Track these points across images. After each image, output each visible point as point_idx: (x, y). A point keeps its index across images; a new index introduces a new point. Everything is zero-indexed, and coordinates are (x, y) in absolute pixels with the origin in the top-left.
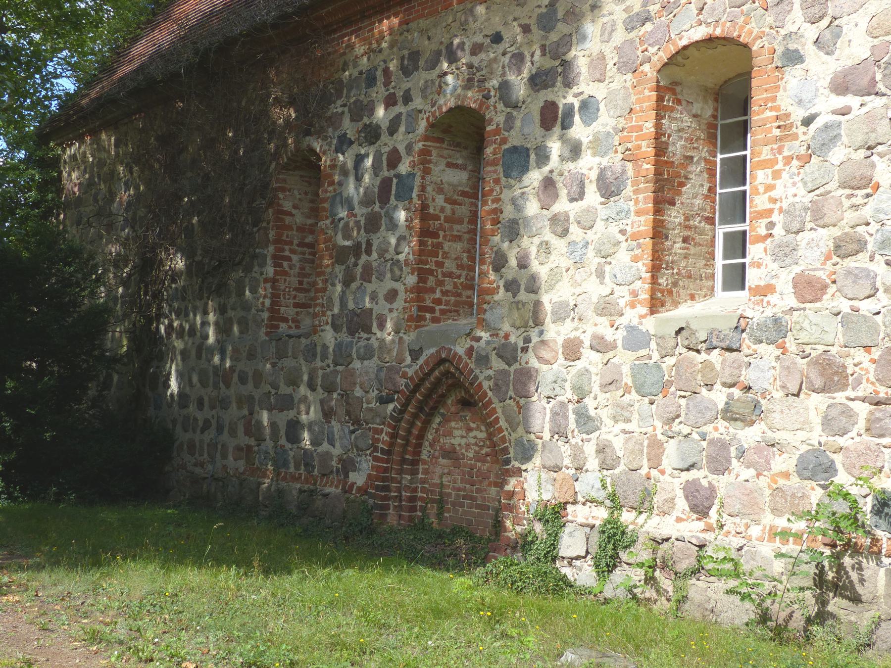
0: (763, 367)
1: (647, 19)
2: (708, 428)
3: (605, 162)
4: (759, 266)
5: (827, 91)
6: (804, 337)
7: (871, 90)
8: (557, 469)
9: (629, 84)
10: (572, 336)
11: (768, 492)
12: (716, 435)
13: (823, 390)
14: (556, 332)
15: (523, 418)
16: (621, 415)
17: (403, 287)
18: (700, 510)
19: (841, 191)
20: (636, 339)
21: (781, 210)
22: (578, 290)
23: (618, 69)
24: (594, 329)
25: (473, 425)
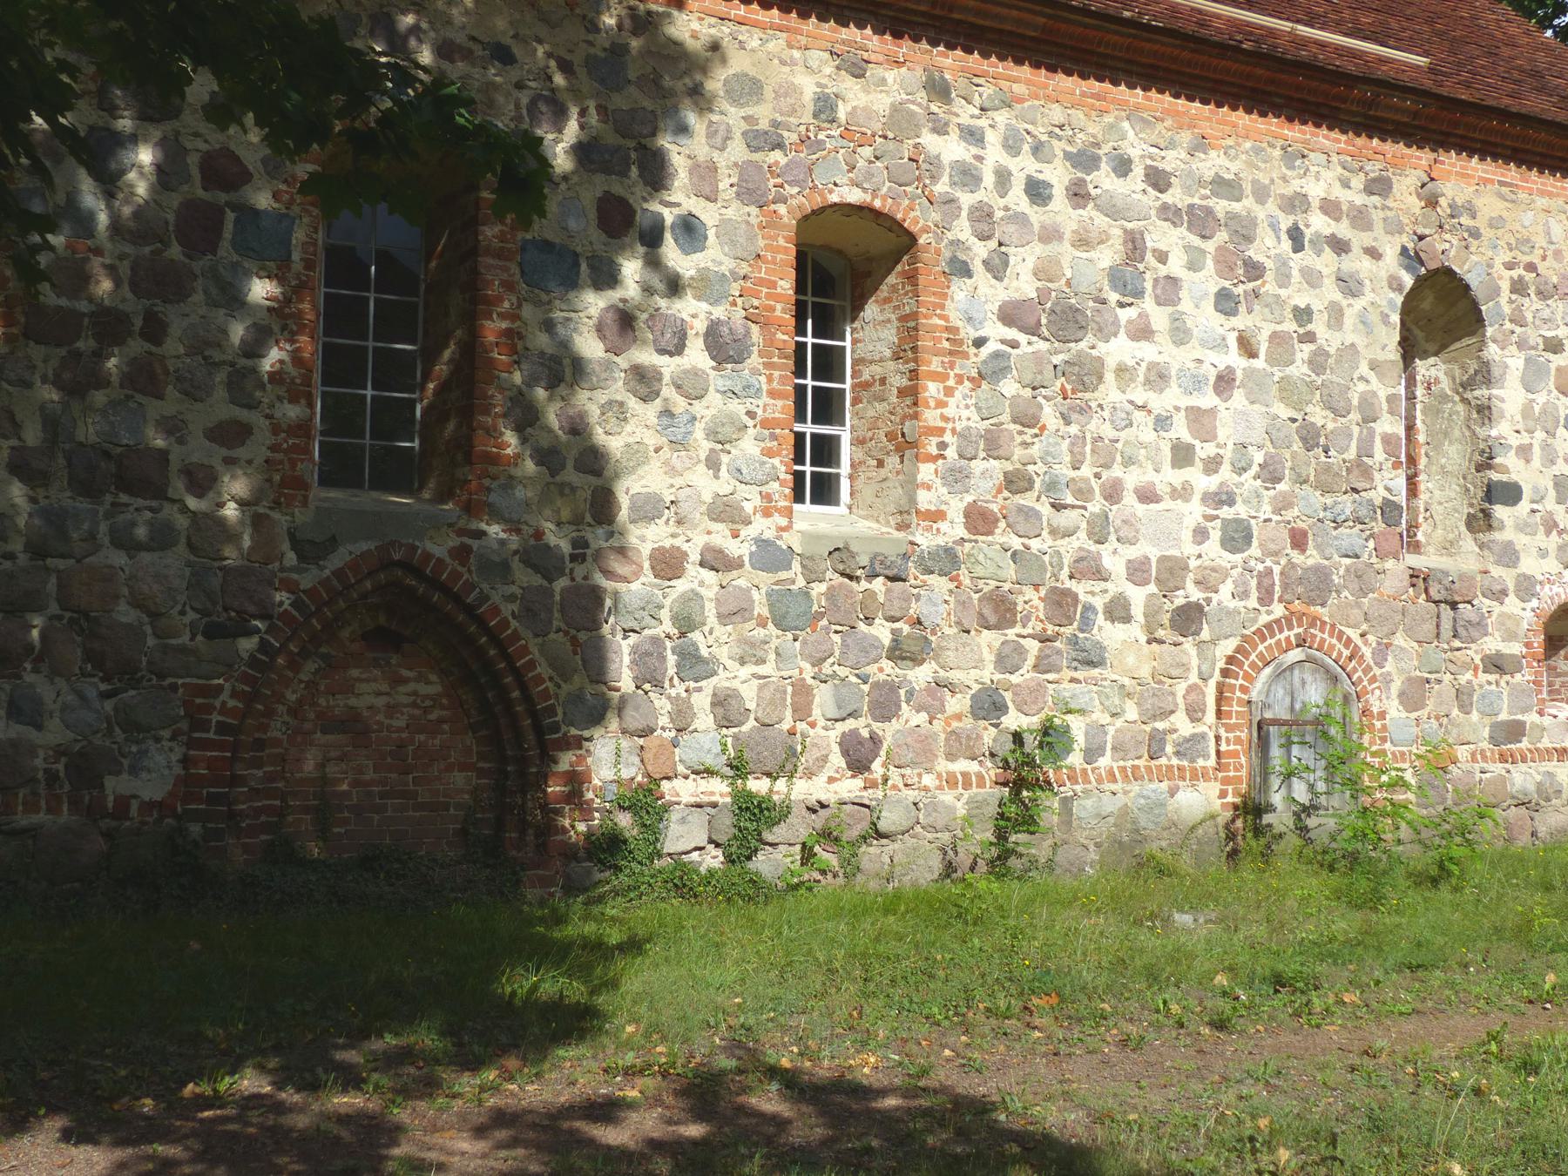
0: (935, 598)
1: (779, 145)
2: (871, 669)
3: (719, 312)
4: (929, 488)
5: (995, 318)
7: (1033, 331)
8: (646, 732)
10: (667, 543)
11: (943, 736)
12: (882, 677)
14: (646, 538)
15: (583, 660)
16: (749, 654)
17: (264, 423)
19: (1012, 427)
20: (770, 556)
21: (954, 431)
22: (678, 482)
23: (738, 194)
24: (706, 538)
25: (405, 673)
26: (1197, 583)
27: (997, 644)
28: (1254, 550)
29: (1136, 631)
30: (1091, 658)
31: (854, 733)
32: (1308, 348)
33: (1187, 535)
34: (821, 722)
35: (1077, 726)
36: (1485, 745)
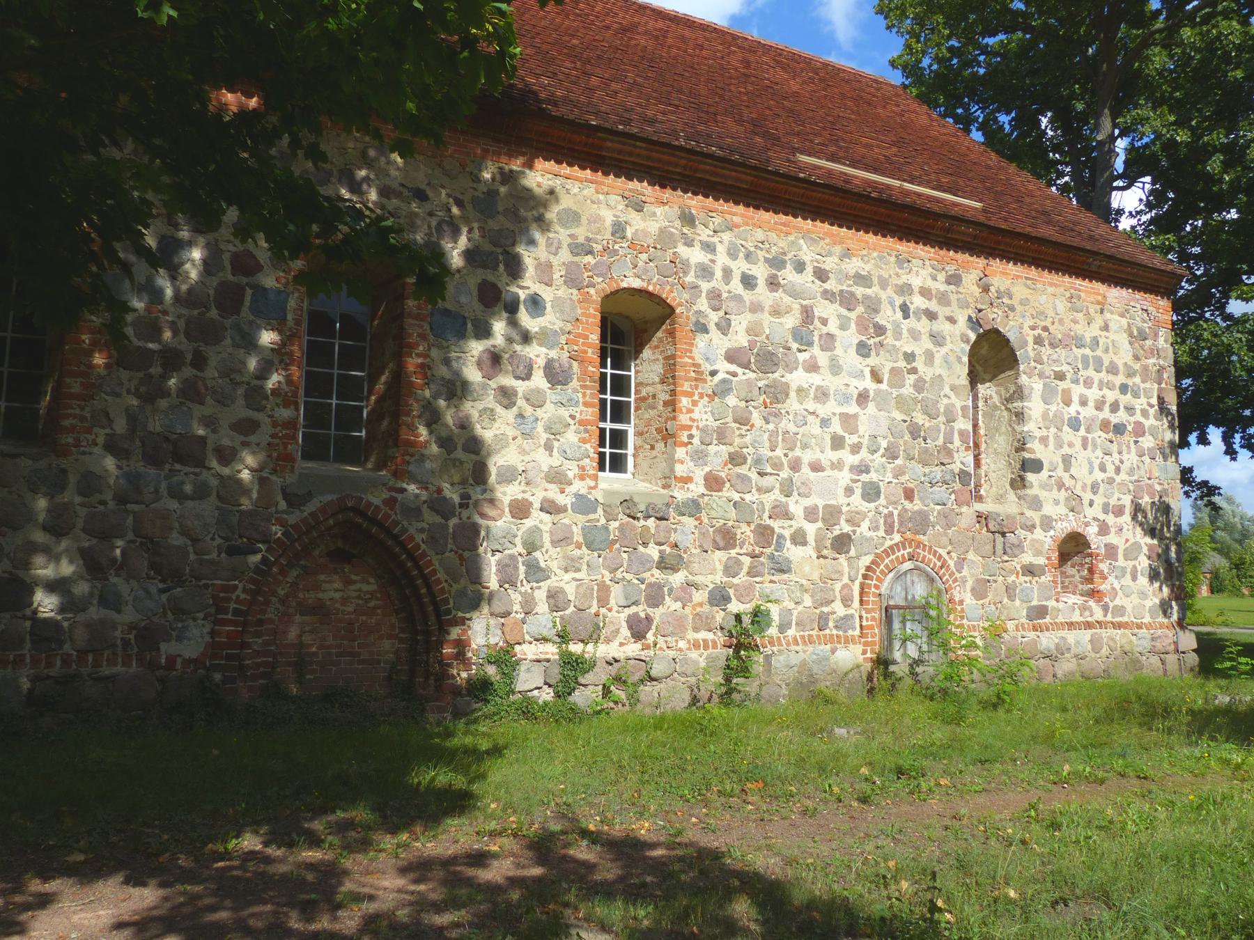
0: (686, 530)
1: (590, 252)
2: (647, 575)
3: (553, 354)
4: (682, 463)
6: (713, 514)
7: (746, 366)
8: (506, 614)
10: (520, 497)
12: (653, 580)
13: (725, 549)
14: (507, 493)
16: (571, 565)
18: (638, 635)
20: (584, 505)
21: (698, 427)
22: (527, 458)
25: (354, 577)
26: (847, 521)
27: (724, 559)
28: (882, 501)
29: (810, 551)
30: (782, 568)
31: (636, 614)
32: (913, 377)
33: (841, 492)
34: (615, 608)
35: (775, 611)
36: (1024, 620)
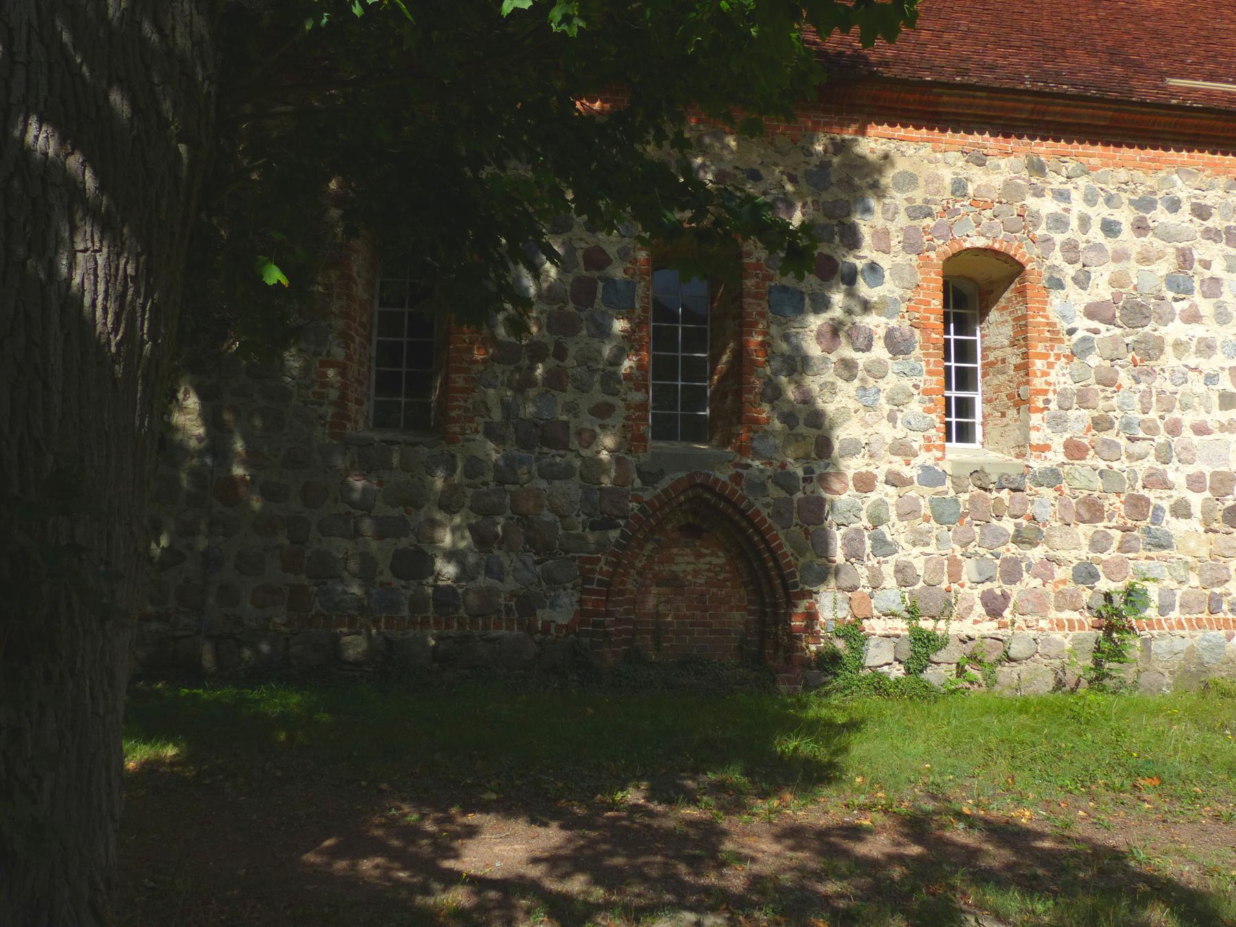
0: (1044, 502)
1: (930, 214)
2: (1001, 550)
3: (893, 323)
4: (1038, 430)
6: (1076, 484)
7: (1110, 321)
9: (914, 263)
10: (864, 470)
11: (1053, 595)
12: (1009, 555)
13: (1090, 521)
14: (852, 466)
17: (621, 404)
19: (1097, 387)
20: (931, 477)
21: (1055, 391)
22: (870, 431)
23: (904, 248)
25: (704, 551)
